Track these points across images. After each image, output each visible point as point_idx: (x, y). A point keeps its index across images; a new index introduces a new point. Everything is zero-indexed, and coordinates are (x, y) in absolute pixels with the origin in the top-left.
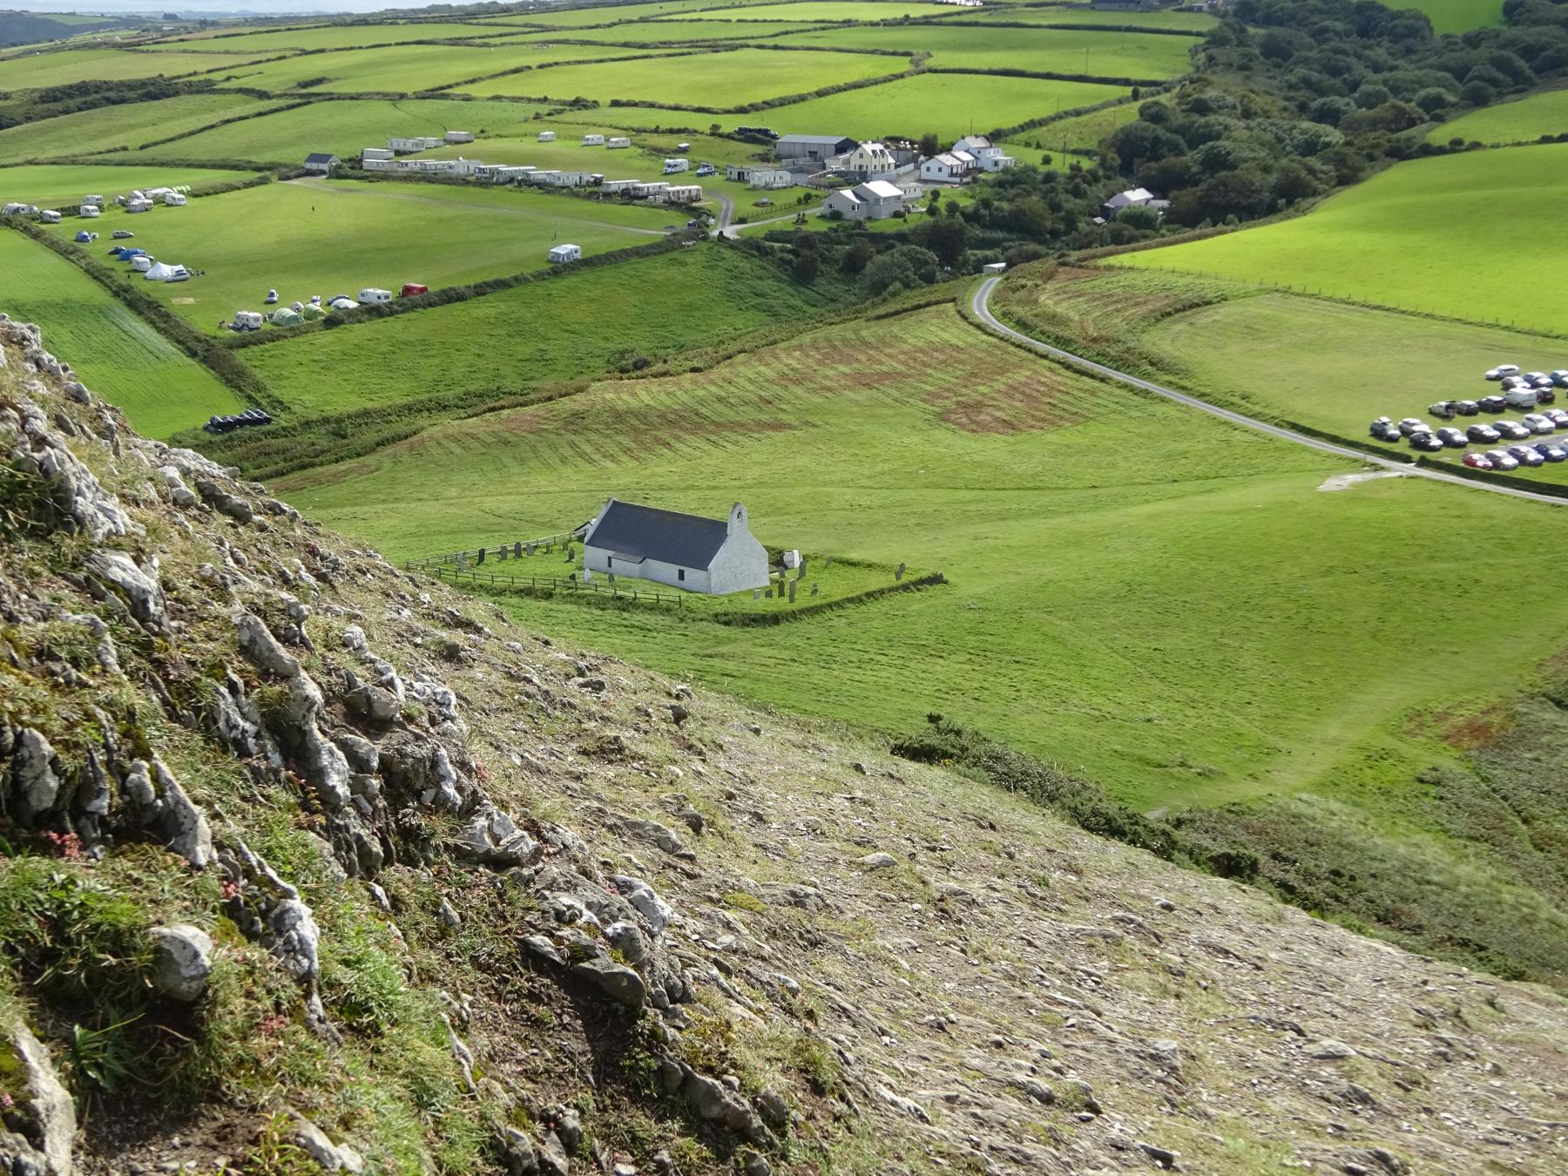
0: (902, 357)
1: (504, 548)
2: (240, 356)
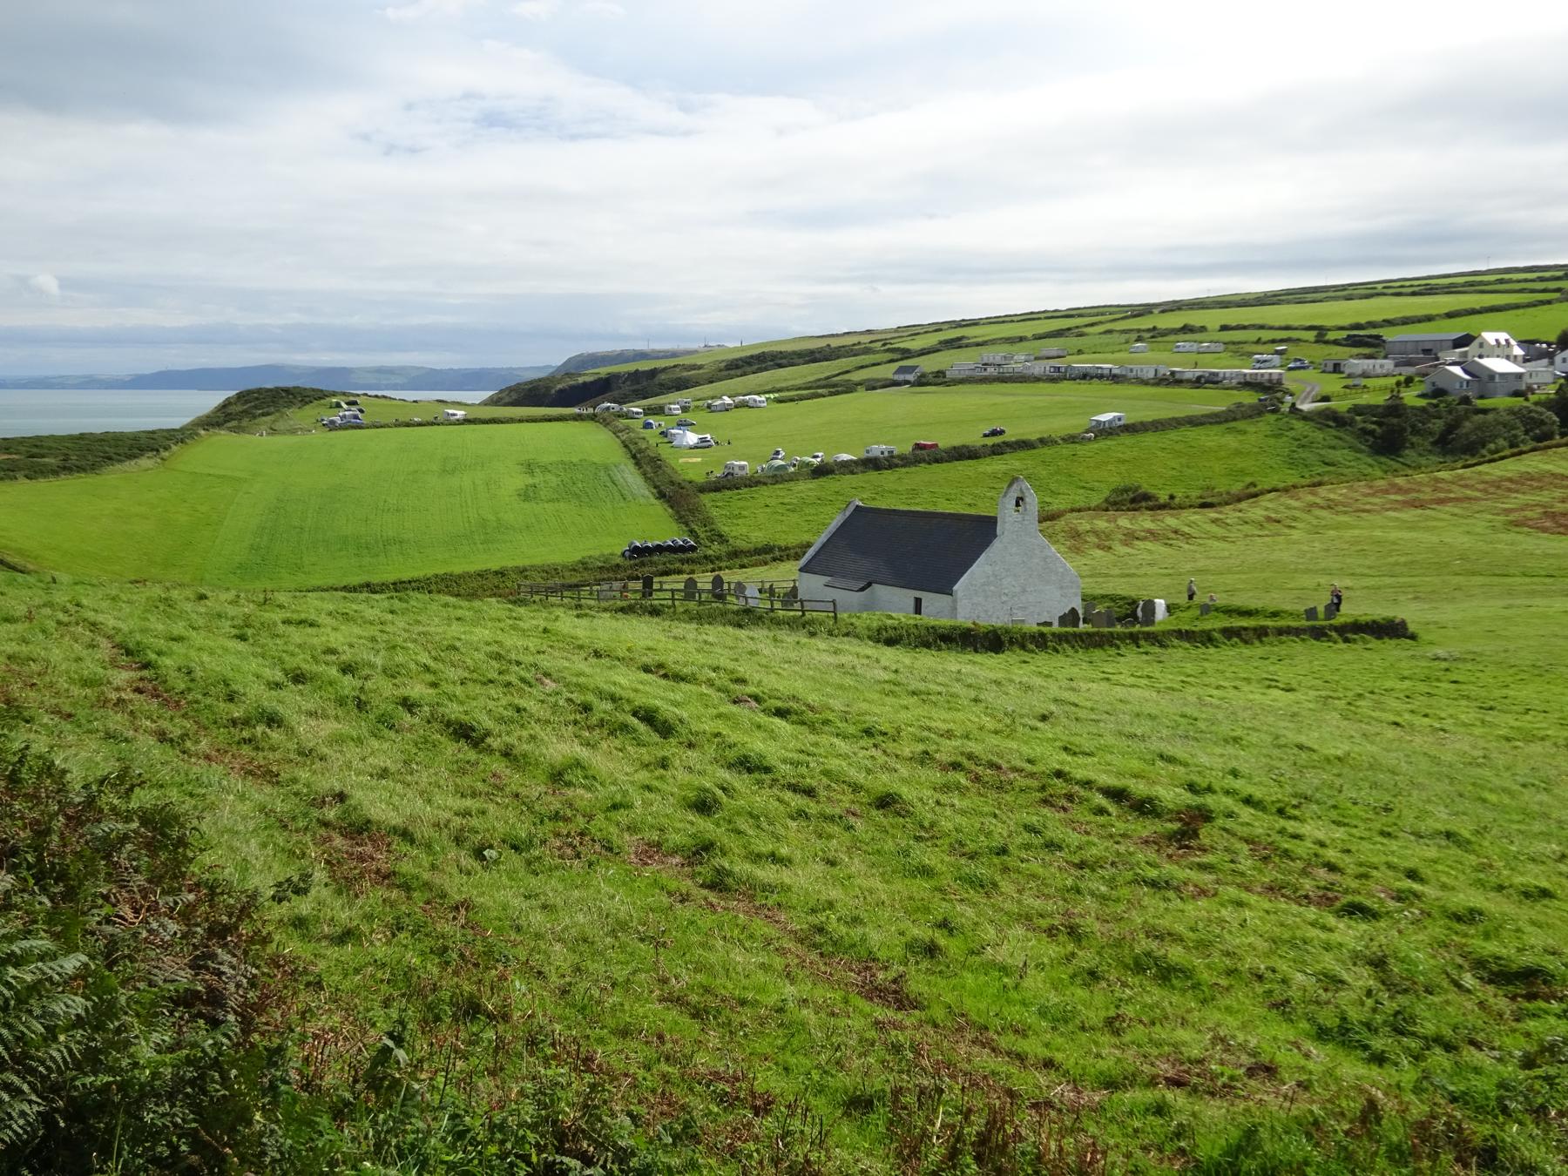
0: (1481, 486)
2: (706, 499)
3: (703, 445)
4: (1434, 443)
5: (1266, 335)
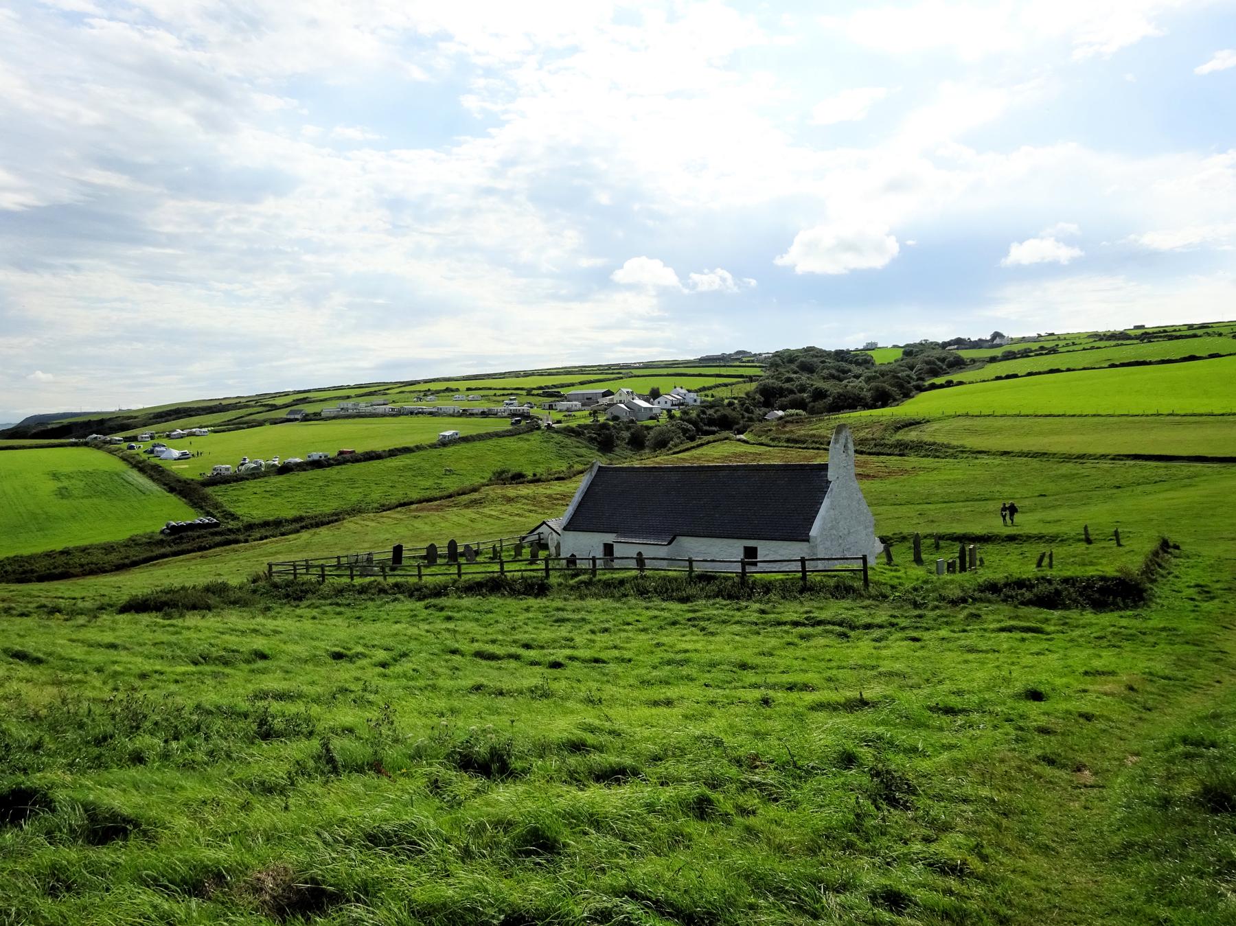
1: (432, 548)
2: (209, 490)
3: (184, 457)
4: (628, 444)
5: (506, 392)
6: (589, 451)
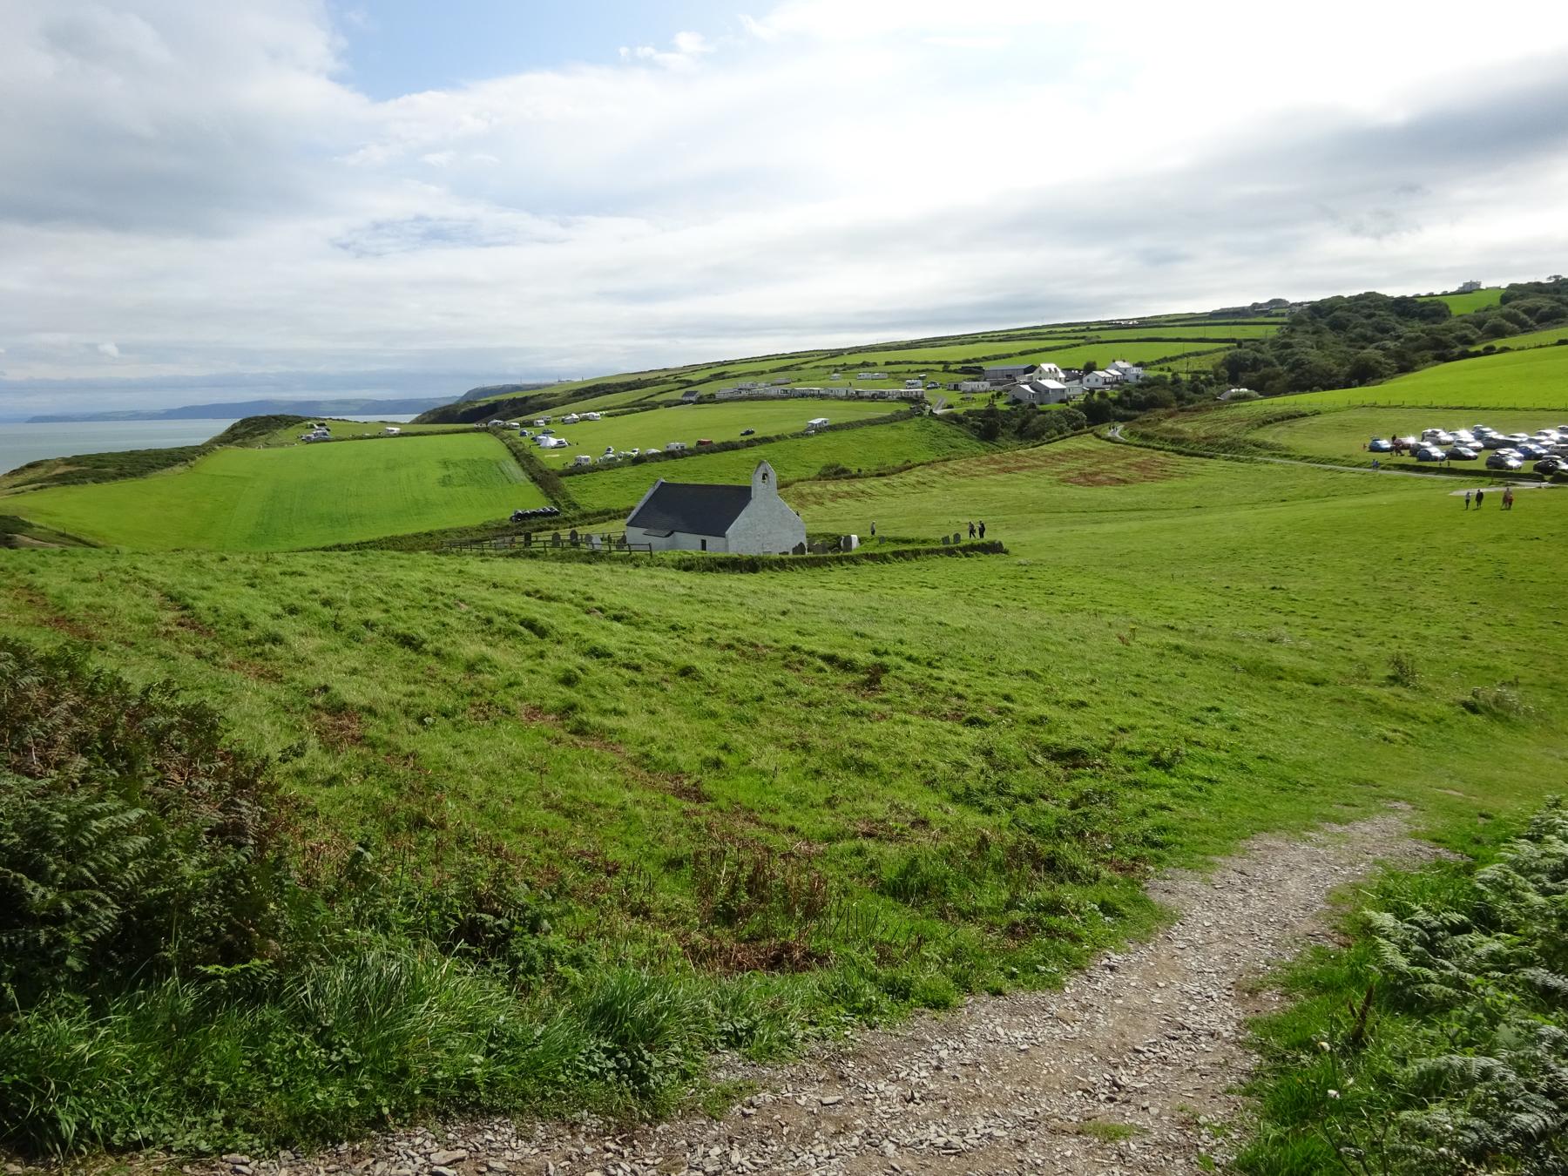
2: (564, 481)
6: (966, 441)
